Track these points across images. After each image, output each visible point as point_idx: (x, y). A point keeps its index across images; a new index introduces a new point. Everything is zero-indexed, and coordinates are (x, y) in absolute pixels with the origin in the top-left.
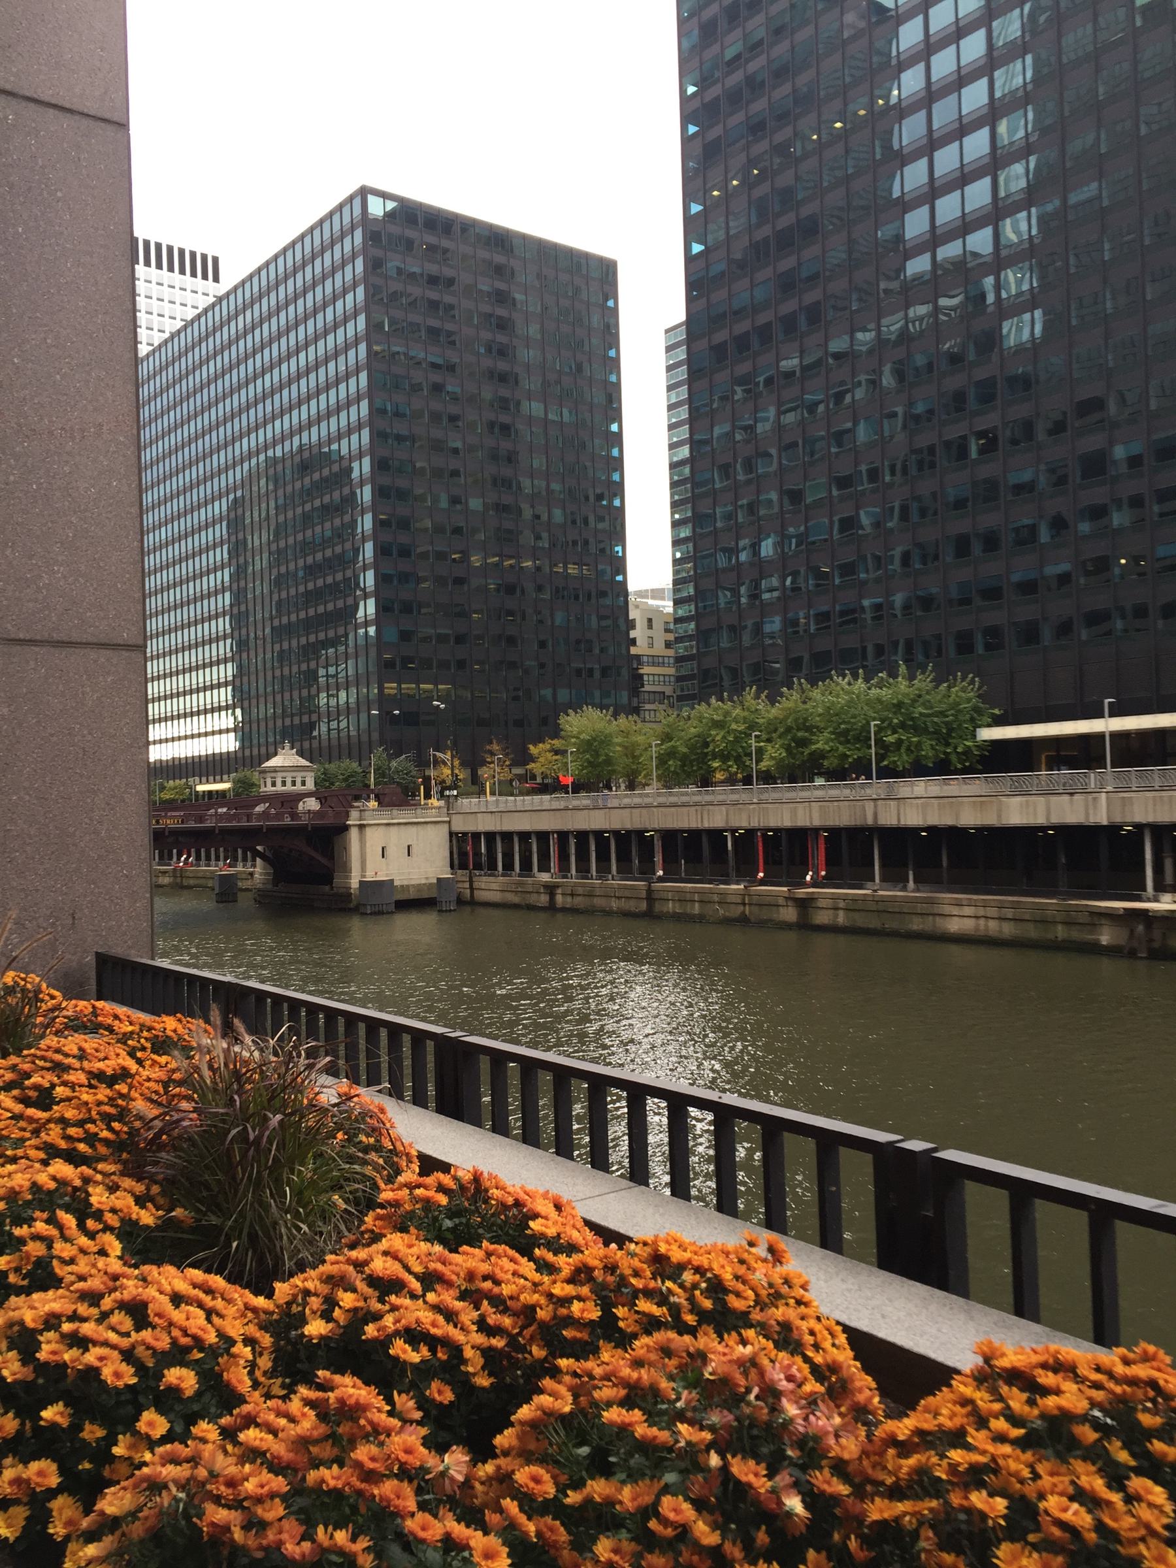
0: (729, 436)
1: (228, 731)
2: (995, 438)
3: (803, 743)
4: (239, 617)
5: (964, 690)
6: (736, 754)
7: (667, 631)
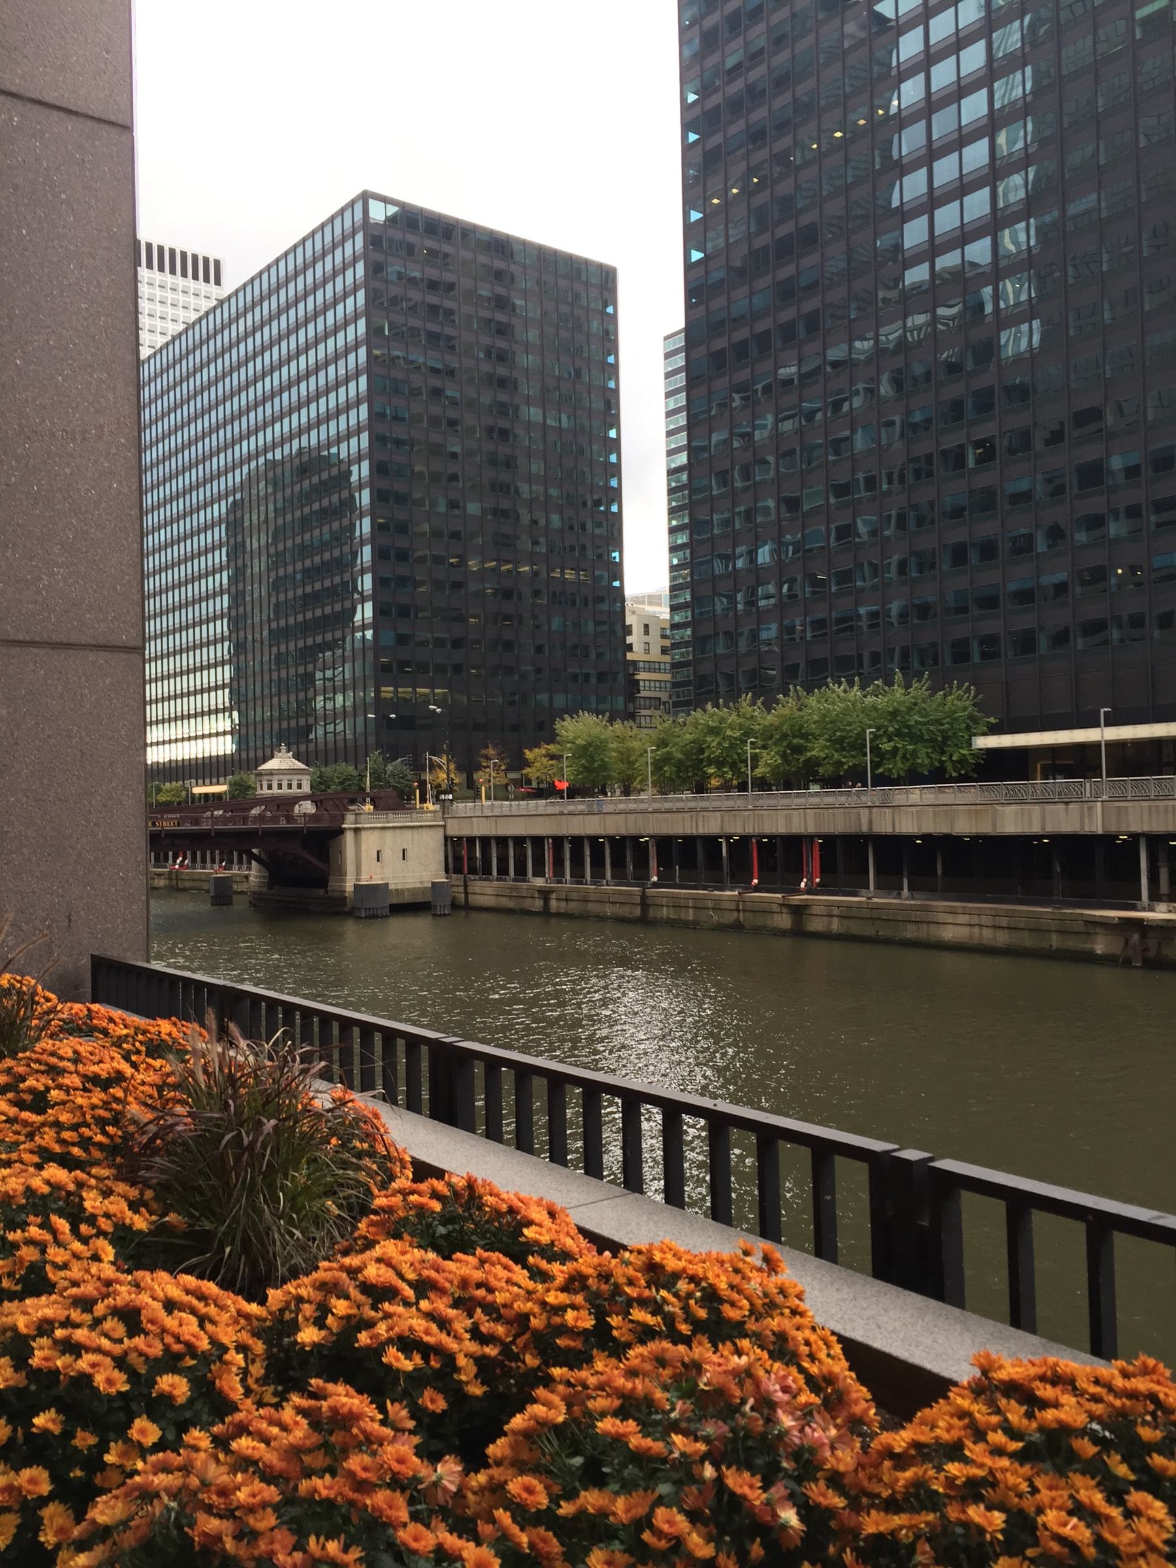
0: (727, 442)
1: (224, 733)
2: (993, 447)
3: (799, 750)
4: (237, 619)
5: (959, 698)
6: (731, 760)
7: (663, 637)
